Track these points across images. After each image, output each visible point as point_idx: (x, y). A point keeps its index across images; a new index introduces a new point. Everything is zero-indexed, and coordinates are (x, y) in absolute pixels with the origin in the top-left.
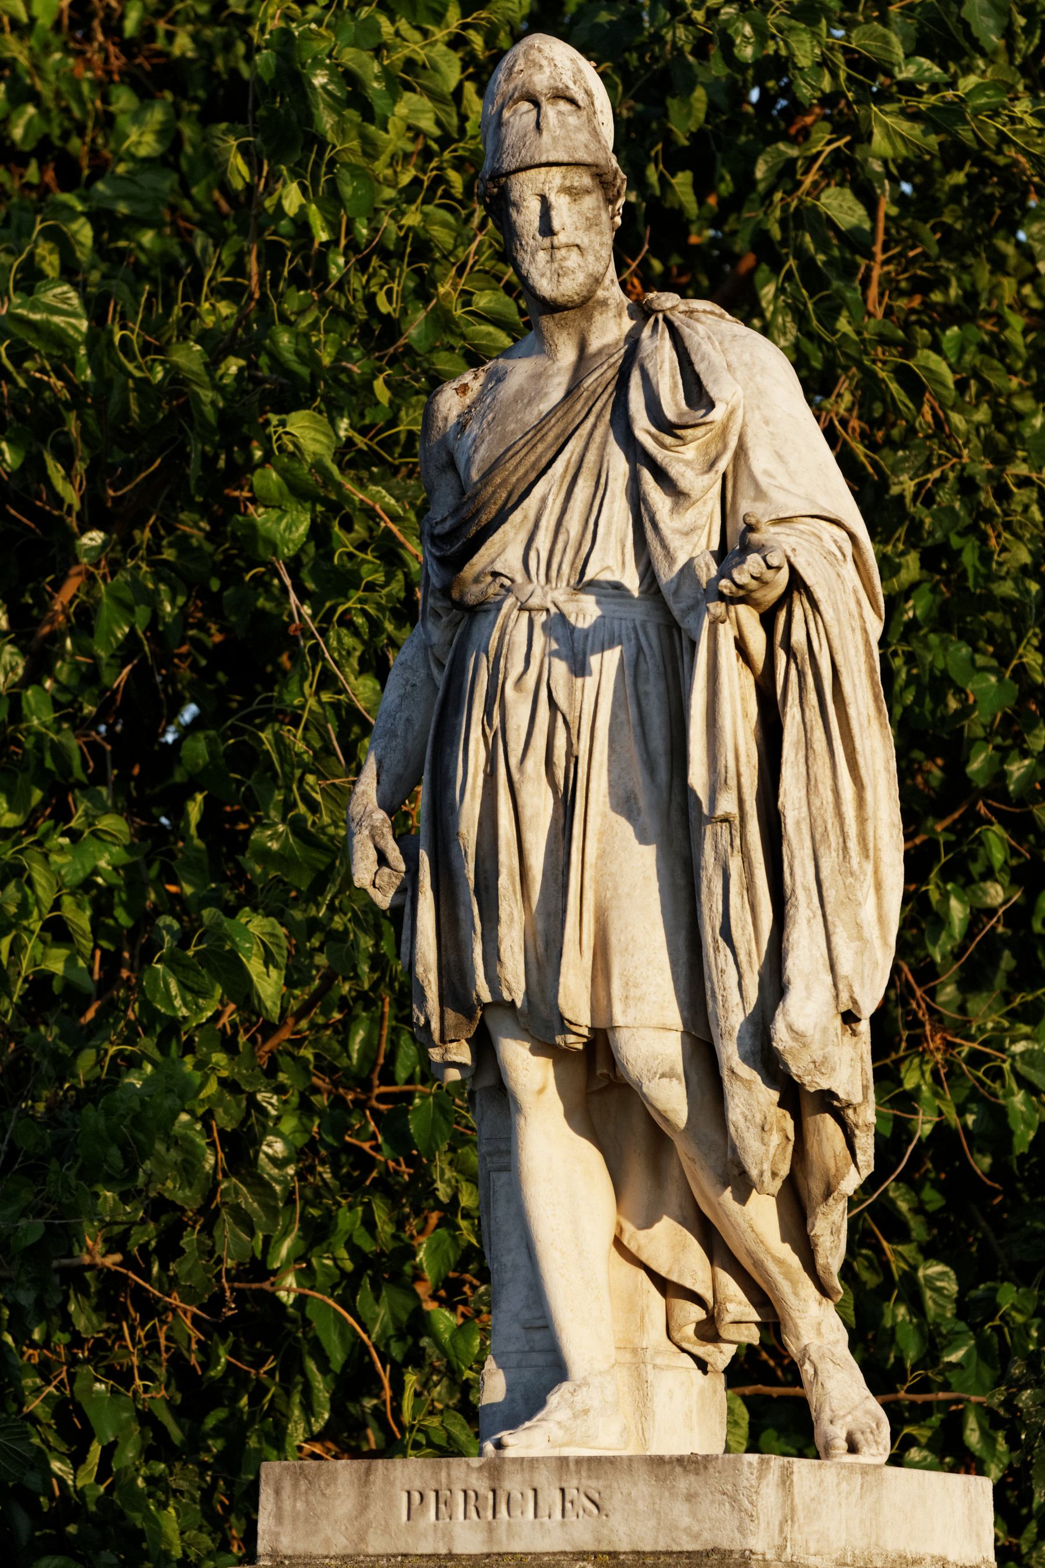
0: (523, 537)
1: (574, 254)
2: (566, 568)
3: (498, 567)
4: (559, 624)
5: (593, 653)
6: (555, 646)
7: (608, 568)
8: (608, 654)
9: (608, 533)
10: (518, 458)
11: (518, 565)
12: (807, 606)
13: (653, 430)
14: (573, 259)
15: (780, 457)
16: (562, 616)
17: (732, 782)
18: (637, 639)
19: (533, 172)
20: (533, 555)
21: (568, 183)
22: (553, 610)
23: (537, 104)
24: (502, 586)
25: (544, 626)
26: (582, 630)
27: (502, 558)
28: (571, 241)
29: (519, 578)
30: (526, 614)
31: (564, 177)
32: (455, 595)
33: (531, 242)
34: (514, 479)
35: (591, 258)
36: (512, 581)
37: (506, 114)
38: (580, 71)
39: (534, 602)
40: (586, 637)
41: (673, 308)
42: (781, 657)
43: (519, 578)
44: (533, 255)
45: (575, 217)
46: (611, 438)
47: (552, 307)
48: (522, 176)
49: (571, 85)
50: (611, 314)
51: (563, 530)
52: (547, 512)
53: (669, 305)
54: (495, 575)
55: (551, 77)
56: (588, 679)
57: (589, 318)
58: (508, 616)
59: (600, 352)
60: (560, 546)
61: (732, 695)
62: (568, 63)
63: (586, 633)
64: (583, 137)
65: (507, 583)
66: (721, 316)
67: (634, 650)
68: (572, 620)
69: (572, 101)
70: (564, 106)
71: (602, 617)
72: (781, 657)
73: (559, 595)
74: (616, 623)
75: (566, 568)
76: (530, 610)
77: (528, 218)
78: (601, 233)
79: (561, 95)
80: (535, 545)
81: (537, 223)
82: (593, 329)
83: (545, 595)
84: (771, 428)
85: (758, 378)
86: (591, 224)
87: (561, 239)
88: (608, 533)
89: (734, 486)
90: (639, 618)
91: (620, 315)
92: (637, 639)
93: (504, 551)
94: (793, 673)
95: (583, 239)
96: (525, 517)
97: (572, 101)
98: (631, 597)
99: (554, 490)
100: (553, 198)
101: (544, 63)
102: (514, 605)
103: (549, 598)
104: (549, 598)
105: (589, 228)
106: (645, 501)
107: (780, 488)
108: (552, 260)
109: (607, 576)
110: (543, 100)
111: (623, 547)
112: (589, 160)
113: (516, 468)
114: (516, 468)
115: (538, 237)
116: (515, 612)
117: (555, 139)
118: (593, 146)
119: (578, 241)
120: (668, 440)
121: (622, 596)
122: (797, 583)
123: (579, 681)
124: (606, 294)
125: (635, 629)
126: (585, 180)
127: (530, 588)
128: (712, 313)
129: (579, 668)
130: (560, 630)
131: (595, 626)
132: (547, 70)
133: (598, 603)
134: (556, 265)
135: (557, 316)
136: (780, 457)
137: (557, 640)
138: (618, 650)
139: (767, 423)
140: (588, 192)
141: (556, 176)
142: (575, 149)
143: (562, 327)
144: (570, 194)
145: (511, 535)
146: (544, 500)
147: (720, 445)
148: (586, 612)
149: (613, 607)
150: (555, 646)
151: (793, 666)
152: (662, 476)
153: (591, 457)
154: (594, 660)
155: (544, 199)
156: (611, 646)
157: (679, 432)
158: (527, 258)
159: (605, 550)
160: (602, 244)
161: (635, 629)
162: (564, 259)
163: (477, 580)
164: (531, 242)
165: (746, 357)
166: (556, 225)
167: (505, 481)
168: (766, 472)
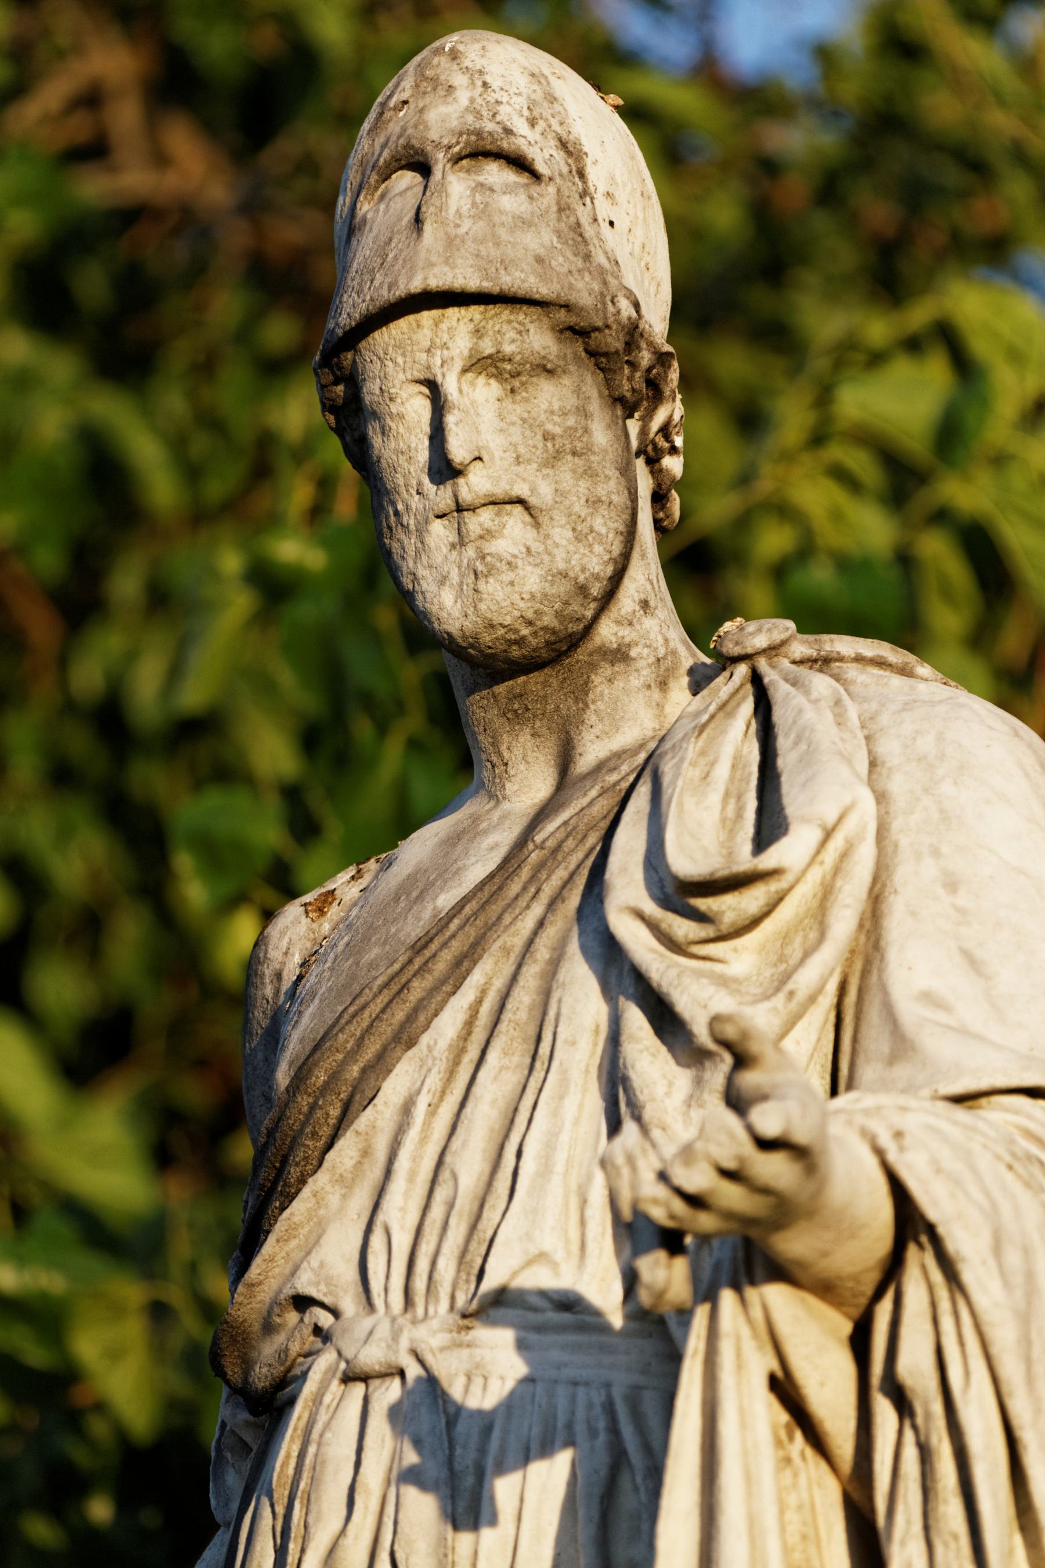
0: (361, 1200)
1: (515, 520)
2: (447, 1268)
3: (305, 1284)
5: (502, 1469)
6: (411, 1457)
7: (542, 1257)
8: (537, 1469)
11: (350, 1273)
12: (937, 1276)
13: (651, 908)
14: (513, 532)
15: (973, 962)
16: (431, 1382)
18: (614, 1430)
19: (402, 325)
20: (377, 1241)
21: (487, 347)
22: (413, 1371)
23: (424, 169)
24: (317, 1330)
25: (395, 1413)
26: (480, 1413)
27: (314, 1260)
28: (500, 490)
29: (349, 1305)
31: (478, 333)
33: (415, 501)
35: (561, 534)
36: (335, 1313)
37: (365, 207)
39: (371, 1357)
40: (487, 1430)
41: (773, 650)
42: (884, 1411)
43: (349, 1305)
44: (421, 532)
45: (516, 434)
48: (383, 338)
49: (521, 126)
50: (635, 682)
52: (413, 1134)
53: (760, 642)
54: (302, 1303)
55: (472, 109)
56: (487, 1534)
57: (581, 692)
58: (317, 1399)
59: (600, 767)
60: (437, 1212)
61: (753, 1522)
62: (522, 82)
63: (486, 1421)
64: (542, 239)
65: (325, 1319)
67: (602, 1459)
68: (456, 1392)
69: (520, 163)
70: (495, 173)
71: (528, 1380)
72: (884, 1411)
73: (432, 1334)
74: (562, 1395)
75: (447, 1268)
76: (365, 1378)
77: (403, 438)
79: (481, 151)
80: (380, 1218)
81: (423, 455)
82: (591, 717)
84: (962, 899)
85: (947, 788)
86: (559, 450)
87: (476, 484)
89: (855, 1040)
90: (621, 1381)
91: (663, 685)
92: (614, 1430)
93: (318, 1240)
94: (910, 1453)
96: (366, 1153)
97: (520, 163)
98: (605, 1328)
99: (434, 1081)
100: (450, 385)
101: (459, 80)
102: (331, 1371)
103: (404, 1343)
104: (404, 1343)
105: (553, 460)
107: (964, 1032)
108: (461, 541)
109: (539, 1279)
110: (440, 161)
111: (584, 1202)
112: (543, 290)
113: (360, 1042)
114: (360, 1042)
115: (429, 487)
116: (335, 1386)
117: (451, 243)
118: (562, 261)
119: (521, 490)
120: (683, 928)
121: (581, 1328)
122: (910, 1222)
123: (464, 1540)
124: (627, 634)
125: (609, 1408)
126: (538, 339)
127: (367, 1322)
128: (880, 663)
129: (467, 1507)
131: (510, 1405)
132: (463, 97)
133: (521, 1346)
134: (470, 552)
136: (973, 962)
137: (417, 1444)
138: (562, 1462)
139: (952, 886)
140: (546, 370)
141: (455, 332)
142: (505, 264)
143: (517, 716)
144: (499, 376)
145: (334, 1200)
146: (407, 1109)
147: (813, 935)
148: (490, 1370)
149: (556, 1355)
150: (411, 1457)
151: (909, 1436)
152: (665, 1019)
153: (524, 998)
154: (504, 1489)
155: (433, 387)
156: (546, 1450)
157: (702, 904)
158: (411, 543)
159: (534, 1213)
161: (609, 1408)
162: (487, 535)
163: (269, 1328)
164: (415, 501)
165: (926, 744)
166: (458, 450)
167: (335, 1076)
168: (928, 997)
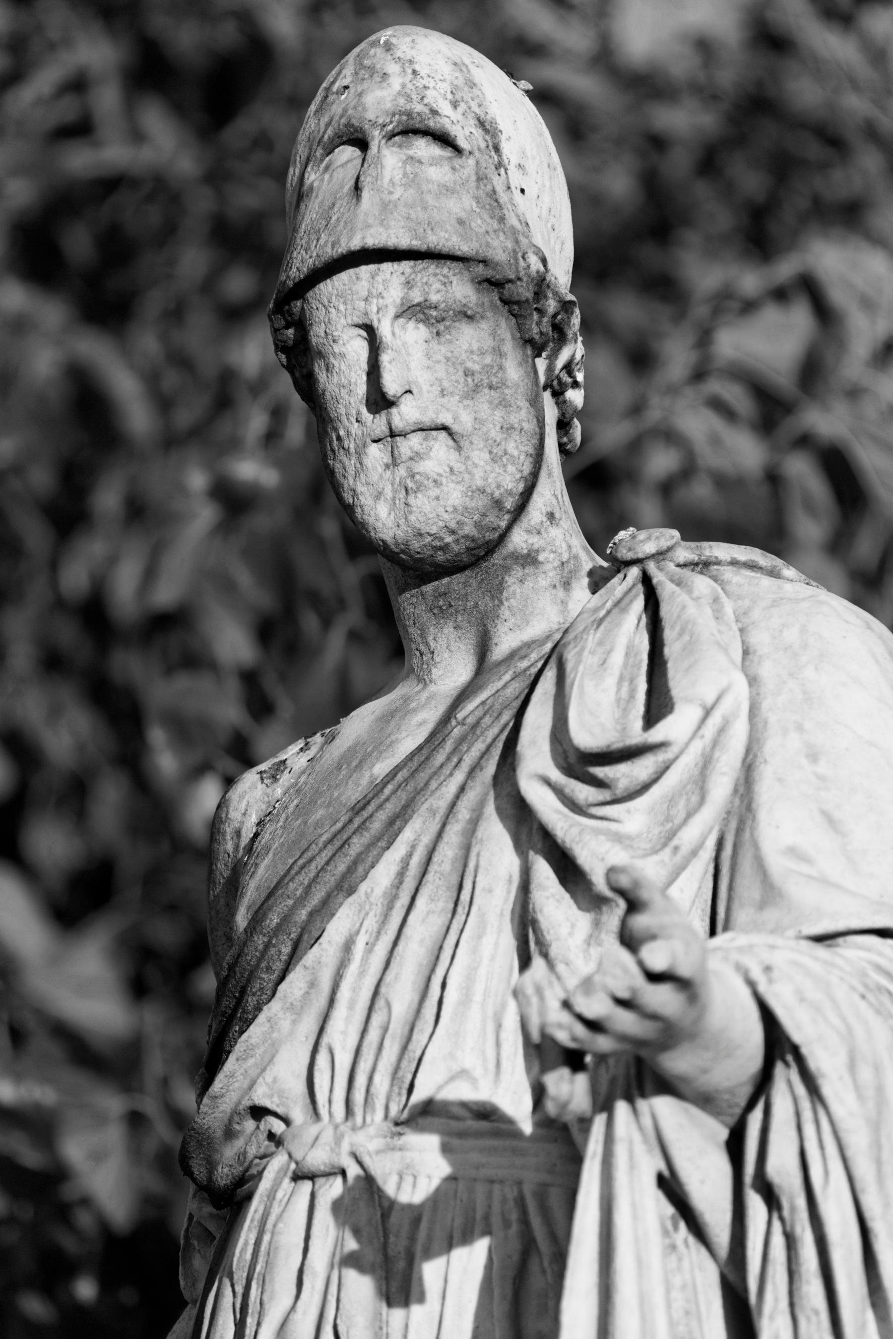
0: (308, 1025)
1: (440, 443)
3: (261, 1097)
4: (367, 1207)
5: (429, 1254)
6: (352, 1244)
7: (463, 1074)
8: (459, 1254)
9: (466, 1000)
10: (313, 869)
12: (801, 1090)
13: (556, 775)
14: (438, 454)
15: (831, 822)
16: (368, 1181)
17: (240, 1276)
18: (525, 1221)
19: (344, 278)
20: (322, 1060)
21: (416, 297)
22: (353, 1171)
23: (363, 144)
24: (271, 1136)
25: (337, 1207)
26: (410, 1206)
27: (268, 1076)
28: (427, 419)
29: (298, 1114)
30: (306, 1187)
31: (409, 284)
32: (199, 1170)
33: (355, 428)
34: (303, 914)
35: (479, 456)
36: (287, 1121)
37: (312, 177)
38: (471, 84)
39: (317, 1159)
40: (416, 1221)
41: (660, 555)
42: (756, 1205)
43: (298, 1114)
44: (360, 454)
45: (441, 371)
46: (490, 809)
47: (421, 568)
48: (327, 288)
49: (445, 108)
51: (380, 1003)
53: (650, 548)
54: (258, 1112)
56: (416, 1310)
57: (497, 591)
59: (513, 655)
62: (446, 70)
63: (416, 1214)
64: (463, 204)
65: (278, 1127)
66: (773, 573)
67: (515, 1246)
68: (390, 1188)
69: (444, 139)
70: (423, 148)
71: (451, 1179)
72: (756, 1205)
74: (480, 1192)
76: (312, 1177)
77: (345, 375)
78: (504, 404)
79: (411, 129)
81: (361, 389)
82: (505, 612)
83: (338, 1140)
84: (822, 768)
85: (809, 673)
87: (406, 413)
88: (466, 1000)
89: (731, 888)
90: (531, 1179)
91: (567, 585)
92: (525, 1221)
93: (271, 1060)
94: (778, 1241)
95: (463, 418)
97: (444, 139)
98: (517, 1134)
99: (371, 923)
100: (385, 329)
101: (392, 68)
102: (283, 1171)
103: (345, 1147)
104: (345, 1147)
106: (534, 923)
107: (824, 881)
108: (394, 462)
110: (376, 138)
111: (499, 1027)
113: (308, 890)
114: (308, 890)
115: (367, 416)
117: (386, 207)
118: (481, 223)
119: (445, 418)
120: (583, 792)
121: (497, 1134)
122: (778, 1044)
123: (397, 1315)
124: (536, 541)
125: (521, 1202)
126: (460, 289)
127: (314, 1129)
128: (752, 566)
129: (399, 1287)
130: (364, 1213)
131: (436, 1200)
132: (396, 83)
133: (446, 1149)
134: (402, 471)
135: (428, 588)
136: (831, 822)
137: (357, 1233)
138: (480, 1249)
139: (813, 756)
140: (467, 316)
141: (389, 283)
143: (442, 611)
144: (426, 321)
145: (285, 1024)
146: (348, 947)
147: (695, 799)
148: (418, 1170)
149: (475, 1157)
150: (352, 1244)
151: (777, 1226)
153: (448, 852)
154: (431, 1272)
155: (370, 330)
156: (467, 1238)
157: (600, 772)
158: (351, 464)
160: (507, 429)
161: (521, 1202)
162: (416, 457)
163: (230, 1134)
164: (355, 428)
165: (792, 635)
167: (286, 919)
168: (793, 852)
